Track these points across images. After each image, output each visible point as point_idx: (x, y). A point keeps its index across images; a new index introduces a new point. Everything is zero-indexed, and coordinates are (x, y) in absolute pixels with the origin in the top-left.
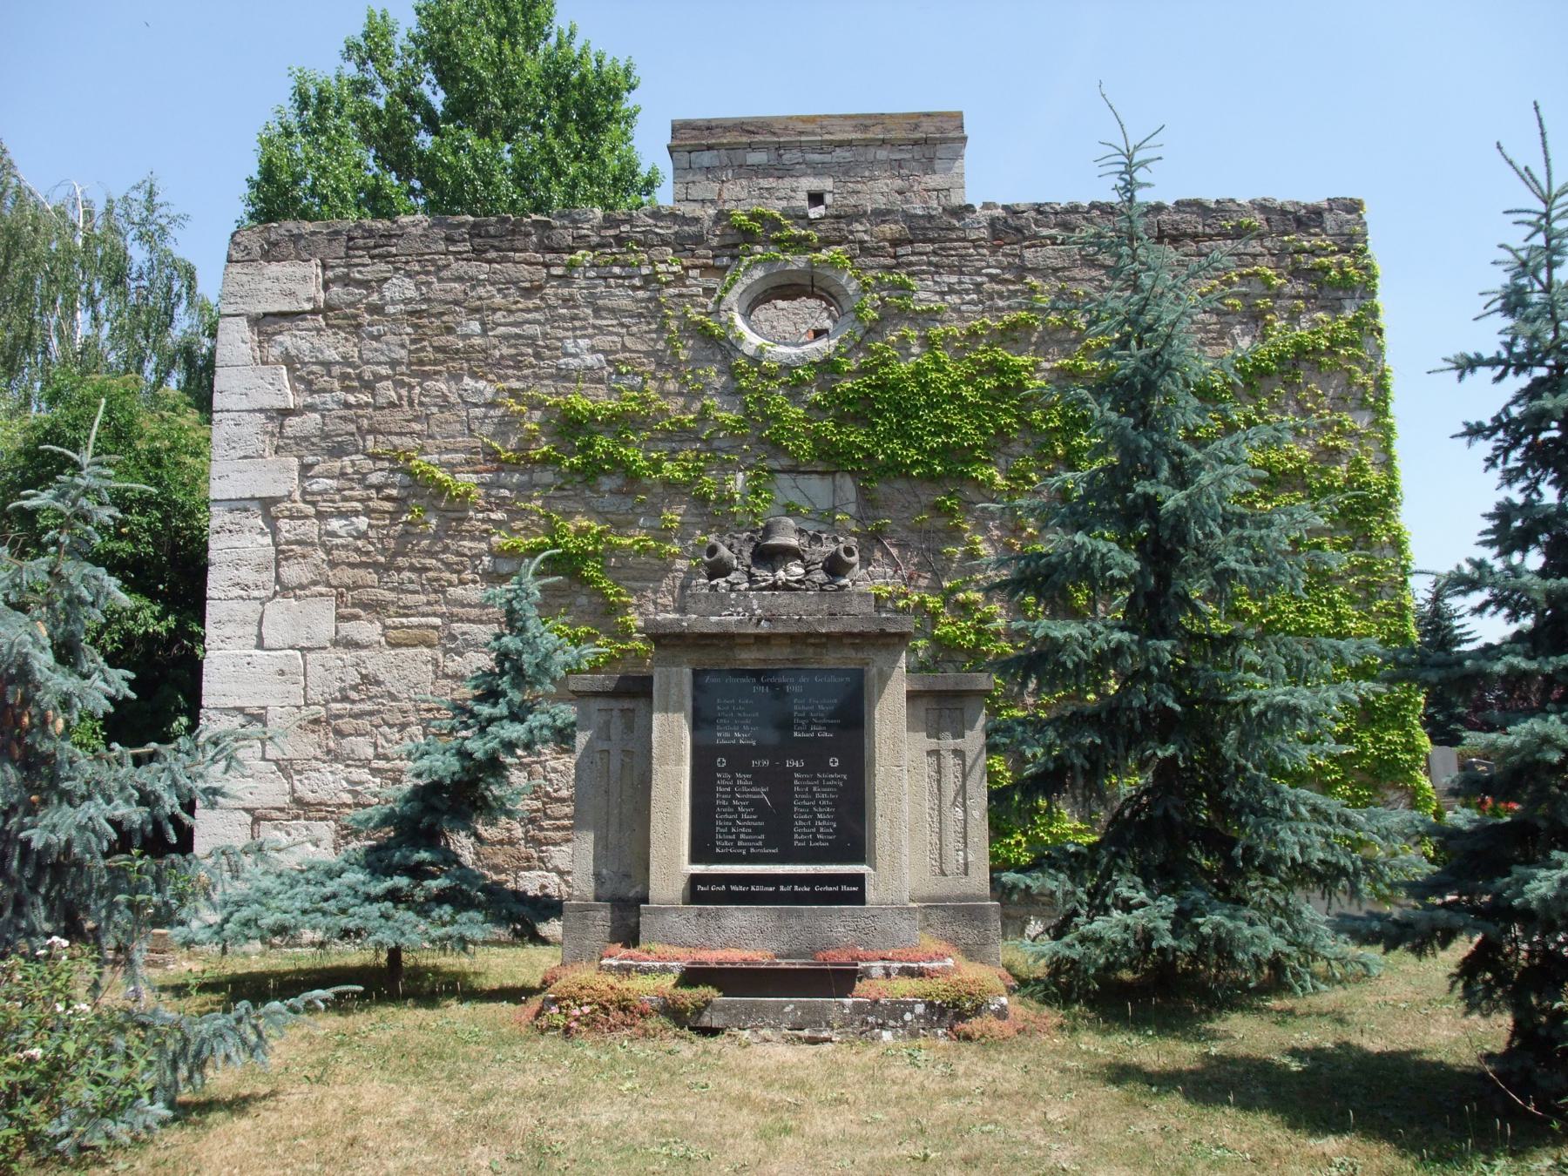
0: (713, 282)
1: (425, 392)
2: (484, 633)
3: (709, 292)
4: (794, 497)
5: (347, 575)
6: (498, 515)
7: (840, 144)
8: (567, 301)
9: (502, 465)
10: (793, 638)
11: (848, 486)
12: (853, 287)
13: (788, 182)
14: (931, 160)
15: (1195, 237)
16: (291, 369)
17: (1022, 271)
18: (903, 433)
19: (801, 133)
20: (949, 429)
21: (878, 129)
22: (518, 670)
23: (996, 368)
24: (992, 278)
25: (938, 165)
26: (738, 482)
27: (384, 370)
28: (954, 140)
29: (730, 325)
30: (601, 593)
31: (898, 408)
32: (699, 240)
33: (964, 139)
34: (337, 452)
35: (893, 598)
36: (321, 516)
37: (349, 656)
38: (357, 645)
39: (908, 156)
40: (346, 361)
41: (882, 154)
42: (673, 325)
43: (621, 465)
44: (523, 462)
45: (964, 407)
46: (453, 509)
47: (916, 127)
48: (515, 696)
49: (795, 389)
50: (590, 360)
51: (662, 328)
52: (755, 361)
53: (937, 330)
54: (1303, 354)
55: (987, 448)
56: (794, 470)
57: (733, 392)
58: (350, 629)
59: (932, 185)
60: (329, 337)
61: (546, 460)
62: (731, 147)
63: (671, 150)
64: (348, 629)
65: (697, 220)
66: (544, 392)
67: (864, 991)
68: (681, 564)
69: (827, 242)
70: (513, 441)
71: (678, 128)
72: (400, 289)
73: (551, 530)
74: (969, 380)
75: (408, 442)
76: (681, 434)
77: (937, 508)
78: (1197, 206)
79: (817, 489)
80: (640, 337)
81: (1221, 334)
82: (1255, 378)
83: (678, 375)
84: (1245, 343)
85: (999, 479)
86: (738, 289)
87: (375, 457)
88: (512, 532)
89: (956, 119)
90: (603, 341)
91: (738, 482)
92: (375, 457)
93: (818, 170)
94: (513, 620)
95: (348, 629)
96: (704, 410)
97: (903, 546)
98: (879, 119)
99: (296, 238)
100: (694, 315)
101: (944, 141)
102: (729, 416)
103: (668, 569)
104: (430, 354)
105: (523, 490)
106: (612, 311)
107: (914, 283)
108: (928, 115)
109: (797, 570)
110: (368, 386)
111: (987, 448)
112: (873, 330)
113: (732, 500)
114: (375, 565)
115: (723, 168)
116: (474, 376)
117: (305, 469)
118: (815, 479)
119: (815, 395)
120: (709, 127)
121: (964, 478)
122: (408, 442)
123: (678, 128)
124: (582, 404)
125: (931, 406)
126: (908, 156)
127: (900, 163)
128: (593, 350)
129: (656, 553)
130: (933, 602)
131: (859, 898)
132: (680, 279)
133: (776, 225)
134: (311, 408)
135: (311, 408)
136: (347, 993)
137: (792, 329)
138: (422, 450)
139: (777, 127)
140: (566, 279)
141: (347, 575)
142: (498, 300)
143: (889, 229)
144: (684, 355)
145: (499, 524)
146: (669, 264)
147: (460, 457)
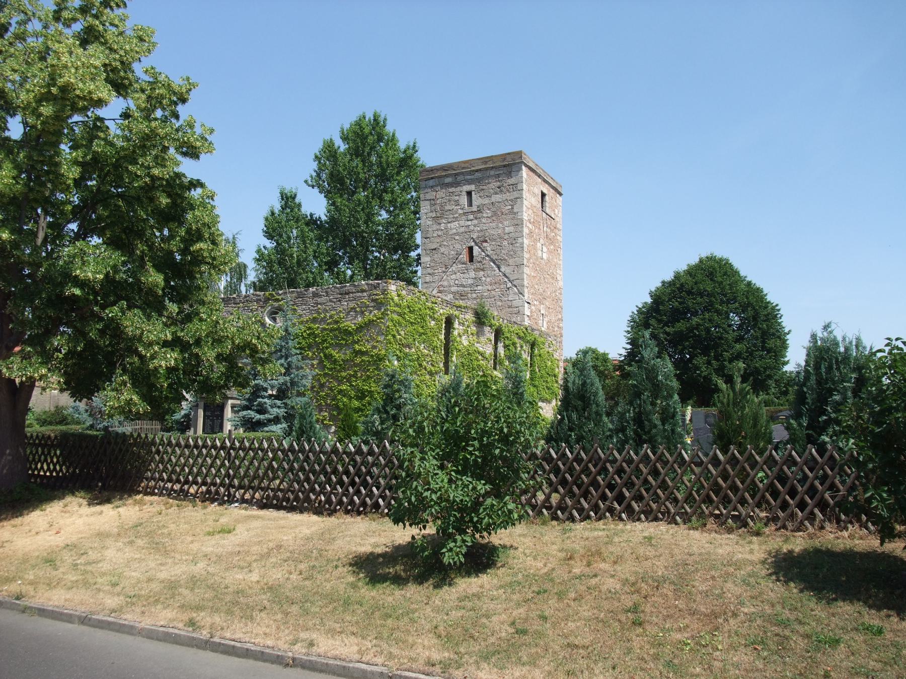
0: (263, 310)
7: (477, 171)
13: (459, 189)
14: (510, 172)
15: (352, 293)
17: (317, 304)
19: (463, 168)
23: (310, 328)
32: (260, 300)
39: (502, 172)
41: (492, 173)
54: (371, 322)
65: (260, 296)
74: (305, 331)
82: (360, 329)
84: (360, 319)
93: (469, 182)
98: (490, 158)
108: (509, 154)
115: (437, 186)
126: (502, 172)
132: (257, 310)
137: (460, 247)
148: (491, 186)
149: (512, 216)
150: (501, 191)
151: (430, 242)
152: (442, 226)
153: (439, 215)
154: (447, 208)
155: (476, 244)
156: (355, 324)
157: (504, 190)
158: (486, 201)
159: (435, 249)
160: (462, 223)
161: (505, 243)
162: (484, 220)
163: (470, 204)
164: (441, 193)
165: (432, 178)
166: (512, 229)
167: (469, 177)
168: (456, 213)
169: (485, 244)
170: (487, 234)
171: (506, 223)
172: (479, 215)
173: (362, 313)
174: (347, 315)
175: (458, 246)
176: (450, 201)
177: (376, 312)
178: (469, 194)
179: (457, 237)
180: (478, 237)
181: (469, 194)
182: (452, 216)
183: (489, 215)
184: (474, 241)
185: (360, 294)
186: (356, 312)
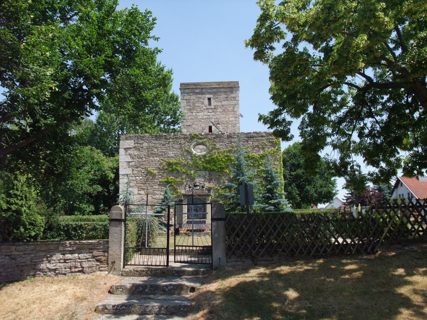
0: (189, 144)
1: (149, 159)
2: (163, 193)
3: (188, 145)
4: (200, 174)
5: (139, 185)
6: (160, 176)
7: (214, 88)
8: (169, 147)
9: (160, 170)
10: (198, 195)
11: (207, 172)
12: (208, 145)
13: (203, 96)
14: (232, 91)
15: (255, 137)
16: (130, 156)
17: (231, 142)
18: (215, 165)
19: (206, 86)
20: (221, 165)
21: (222, 85)
22: (167, 198)
23: (227, 156)
24: (227, 143)
25: (234, 92)
26: (192, 172)
27: (144, 156)
28: (237, 87)
29: (191, 150)
30: (174, 187)
31: (214, 162)
32: (187, 138)
33: (239, 87)
34: (137, 168)
35: (213, 187)
36: (135, 176)
37: (140, 196)
38: (141, 194)
40: (138, 155)
41: (222, 90)
42: (183, 150)
43: (177, 170)
44: (163, 169)
45: (223, 161)
46: (154, 176)
47: (229, 84)
48: (167, 202)
49: (200, 159)
50: (172, 155)
51: (182, 150)
52: (195, 155)
53: (219, 151)
55: (226, 167)
56: (200, 170)
57: (192, 159)
58: (140, 192)
59: (233, 96)
60: (135, 151)
61: (166, 169)
62: (192, 89)
63: (180, 89)
64: (140, 192)
66: (166, 159)
67: (205, 232)
68: (185, 183)
69: (205, 138)
70: (162, 166)
71: (181, 85)
72: (145, 145)
73: (167, 179)
74: (224, 158)
75: (147, 166)
76: (185, 165)
77: (219, 175)
78: (256, 133)
79: (203, 172)
80: (179, 152)
81: (259, 151)
83: (184, 157)
84: (262, 152)
85: (228, 171)
86: (192, 145)
87: (143, 168)
88: (162, 179)
89: (237, 83)
90: (174, 152)
91: (192, 172)
92: (143, 168)
94: (166, 193)
95: (140, 192)
96: (188, 162)
97: (215, 180)
98: (222, 83)
99: (130, 137)
100: (186, 149)
101: (235, 87)
102: (191, 163)
103: (183, 184)
104: (150, 154)
105: (163, 173)
106: (175, 148)
107: (216, 144)
108: (232, 82)
109: (199, 187)
110: (141, 158)
111: (226, 167)
112: (211, 151)
113: (192, 175)
114: (143, 183)
115: (191, 93)
116: (156, 157)
117: (133, 170)
118: (203, 172)
119: (203, 160)
120: (188, 84)
121: (223, 171)
122: (147, 166)
123: (181, 85)
124: (171, 161)
125: (219, 162)
127: (226, 92)
128: (173, 153)
129: (182, 182)
130: (219, 188)
131: (205, 223)
132: (184, 144)
133: (197, 136)
134: (133, 161)
135: (133, 161)
136: (145, 237)
138: (149, 167)
139: (201, 84)
140: (169, 143)
141: (139, 185)
142: (159, 146)
143: (213, 136)
144: (185, 154)
145: (160, 178)
146: (183, 141)
147: (154, 168)
148: (222, 96)
149: (233, 113)
150: (227, 100)
151: (187, 122)
152: (194, 114)
153: (191, 108)
154: (197, 105)
155: (214, 125)
156: (258, 154)
157: (229, 100)
158: (219, 104)
159: (189, 126)
160: (205, 113)
161: (230, 126)
162: (218, 113)
163: (210, 104)
164: (193, 97)
165: (188, 89)
166: (233, 119)
167: (209, 91)
168: (202, 108)
169: (218, 125)
170: (220, 120)
171: (230, 116)
172: (215, 110)
173: (263, 148)
174: (253, 149)
175: (203, 125)
176: (198, 101)
177: (272, 148)
178: (209, 99)
179: (203, 121)
180: (215, 121)
181: (209, 99)
182: (199, 109)
183: (221, 111)
184: (212, 123)
185: (260, 138)
186: (259, 148)
